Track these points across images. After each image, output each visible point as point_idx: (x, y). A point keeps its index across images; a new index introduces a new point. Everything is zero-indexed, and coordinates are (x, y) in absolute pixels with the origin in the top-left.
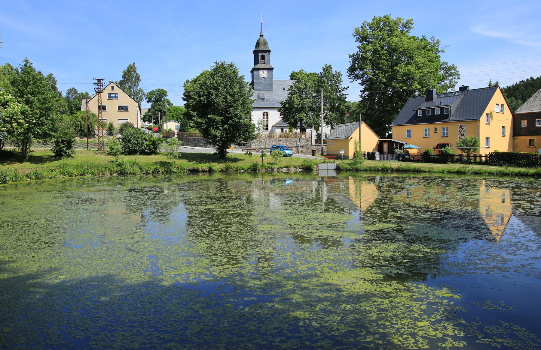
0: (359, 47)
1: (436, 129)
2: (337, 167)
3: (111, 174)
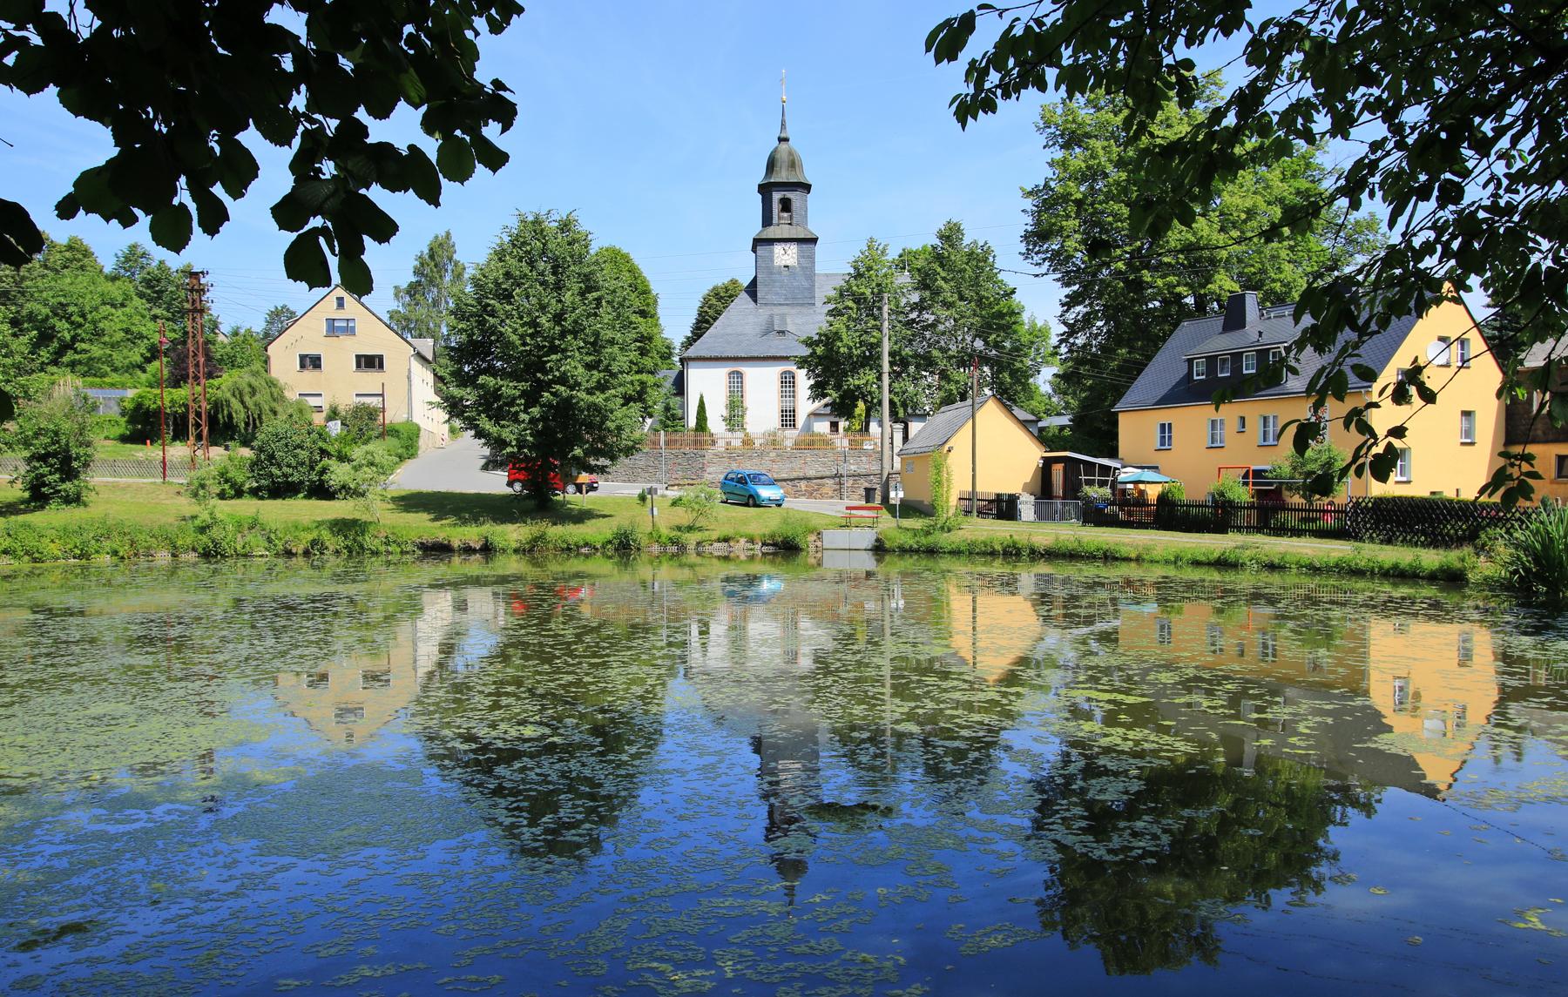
0: (1051, 164)
1: (1243, 419)
2: (878, 540)
3: (174, 555)
